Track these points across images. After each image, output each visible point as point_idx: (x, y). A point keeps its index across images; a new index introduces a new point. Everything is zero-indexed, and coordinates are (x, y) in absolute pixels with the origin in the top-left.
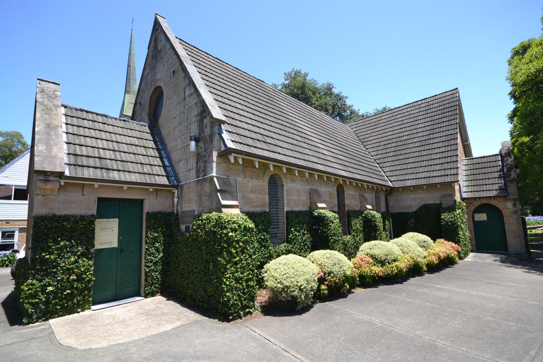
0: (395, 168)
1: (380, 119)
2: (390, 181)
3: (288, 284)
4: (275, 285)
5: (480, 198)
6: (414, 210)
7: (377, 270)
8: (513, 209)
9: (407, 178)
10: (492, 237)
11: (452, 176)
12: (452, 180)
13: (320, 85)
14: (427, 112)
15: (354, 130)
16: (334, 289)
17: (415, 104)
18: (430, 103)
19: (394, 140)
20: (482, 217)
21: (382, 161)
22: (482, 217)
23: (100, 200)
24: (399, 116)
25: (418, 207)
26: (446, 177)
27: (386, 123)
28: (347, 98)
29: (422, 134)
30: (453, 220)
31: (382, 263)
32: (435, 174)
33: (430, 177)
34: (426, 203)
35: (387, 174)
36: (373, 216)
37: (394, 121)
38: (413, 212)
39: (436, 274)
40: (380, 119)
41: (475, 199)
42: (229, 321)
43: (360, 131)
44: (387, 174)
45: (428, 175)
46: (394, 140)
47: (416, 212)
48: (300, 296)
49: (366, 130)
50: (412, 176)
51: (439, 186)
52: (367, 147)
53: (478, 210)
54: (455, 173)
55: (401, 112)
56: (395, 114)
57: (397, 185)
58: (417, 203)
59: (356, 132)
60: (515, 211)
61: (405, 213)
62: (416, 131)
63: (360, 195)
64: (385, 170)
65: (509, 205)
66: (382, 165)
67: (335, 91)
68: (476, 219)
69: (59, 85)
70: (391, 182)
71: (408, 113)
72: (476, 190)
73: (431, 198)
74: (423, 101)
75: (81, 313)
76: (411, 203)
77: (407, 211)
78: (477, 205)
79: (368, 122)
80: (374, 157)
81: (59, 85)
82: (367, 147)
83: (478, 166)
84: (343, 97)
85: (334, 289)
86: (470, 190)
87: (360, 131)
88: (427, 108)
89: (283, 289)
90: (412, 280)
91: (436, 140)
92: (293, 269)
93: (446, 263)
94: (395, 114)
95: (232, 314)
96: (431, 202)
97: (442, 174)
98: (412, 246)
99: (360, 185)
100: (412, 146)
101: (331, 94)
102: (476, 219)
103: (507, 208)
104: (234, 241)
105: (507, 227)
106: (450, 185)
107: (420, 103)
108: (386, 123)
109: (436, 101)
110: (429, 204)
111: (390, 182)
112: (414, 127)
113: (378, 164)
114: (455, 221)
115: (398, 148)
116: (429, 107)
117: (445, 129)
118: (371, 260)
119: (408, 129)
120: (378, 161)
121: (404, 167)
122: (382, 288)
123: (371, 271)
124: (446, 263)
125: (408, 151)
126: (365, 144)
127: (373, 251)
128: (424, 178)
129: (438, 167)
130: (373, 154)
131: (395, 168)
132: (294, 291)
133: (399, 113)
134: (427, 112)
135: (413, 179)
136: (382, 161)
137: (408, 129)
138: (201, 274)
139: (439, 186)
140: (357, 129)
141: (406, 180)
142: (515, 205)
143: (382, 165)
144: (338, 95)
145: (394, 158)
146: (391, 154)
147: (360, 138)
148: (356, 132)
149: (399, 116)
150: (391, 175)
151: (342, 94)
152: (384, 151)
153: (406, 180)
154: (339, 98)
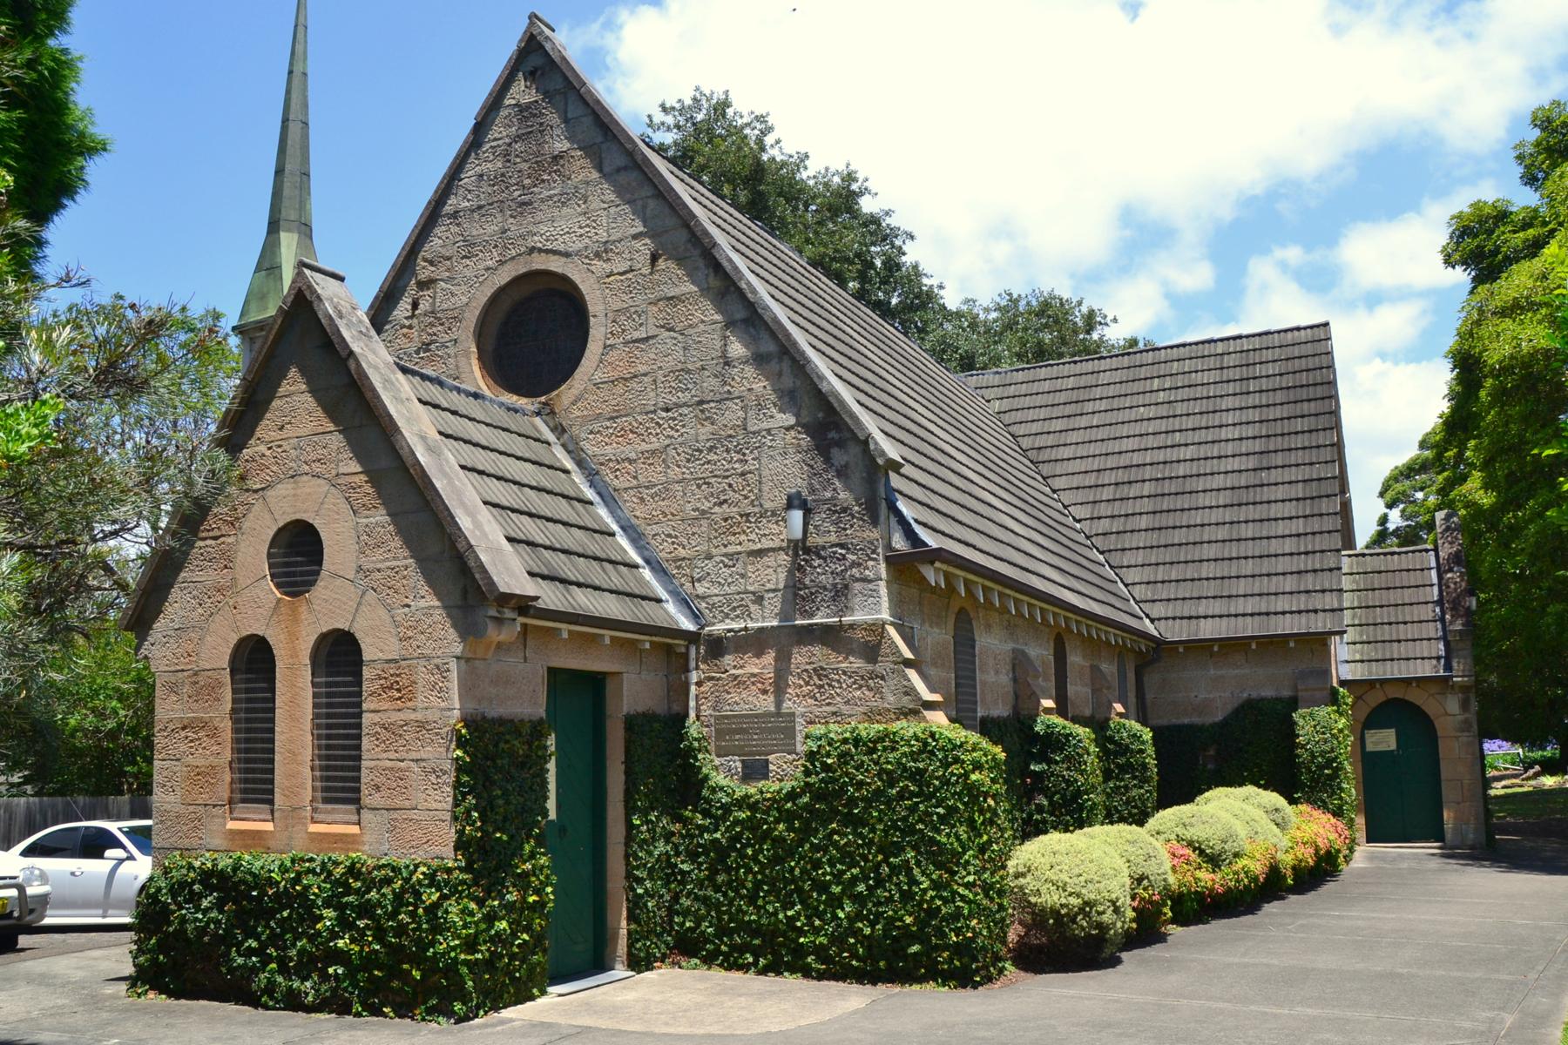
0: (1161, 574)
1: (1090, 380)
2: (1147, 616)
3: (1092, 896)
4: (1063, 901)
5: (1383, 682)
6: (1219, 717)
7: (1206, 878)
8: (1461, 718)
9: (1201, 611)
10: (1402, 802)
11: (1328, 615)
12: (1329, 627)
13: (811, 172)
14: (1244, 387)
15: (997, 405)
16: (1159, 916)
17: (1207, 350)
18: (1252, 357)
19: (1148, 473)
20: (1384, 740)
21: (1112, 542)
22: (1384, 740)
23: (552, 671)
24: (1156, 383)
25: (1229, 708)
26: (1312, 615)
27: (1116, 403)
28: (912, 238)
29: (1235, 464)
30: (1327, 747)
31: (1214, 861)
32: (1282, 604)
33: (1267, 614)
34: (1254, 695)
35: (1137, 591)
36: (1136, 737)
37: (1140, 399)
38: (1213, 725)
39: (1311, 895)
40: (1090, 380)
41: (1371, 684)
42: (975, 986)
43: (1019, 416)
44: (1138, 591)
45: (1263, 605)
46: (1148, 473)
47: (1225, 723)
48: (1114, 924)
49: (1043, 413)
50: (1217, 607)
51: (1292, 644)
52: (1058, 483)
53: (1373, 720)
54: (1336, 606)
55: (1163, 369)
56: (1143, 372)
57: (1175, 632)
58: (1227, 694)
59: (1007, 418)
60: (1466, 721)
61: (1191, 727)
62: (1215, 450)
63: (1092, 667)
64: (1132, 576)
65: (1453, 704)
66: (1116, 559)
67: (867, 205)
68: (1370, 748)
69: (342, 279)
70: (1152, 621)
71: (1186, 380)
72: (1373, 655)
73: (1264, 682)
74: (1232, 346)
75: (539, 1001)
76: (1212, 696)
77: (1196, 720)
78: (1373, 705)
79: (1046, 386)
80: (1085, 526)
81: (342, 279)
82: (1058, 483)
83: (1377, 581)
84: (894, 232)
85: (1159, 916)
86: (1358, 657)
87: (1019, 416)
88: (1245, 372)
89: (1082, 910)
90: (1271, 908)
91: (1280, 492)
92: (1082, 863)
93: (1319, 872)
94: (1143, 372)
95: (977, 971)
96: (1268, 693)
97: (1302, 607)
98: (1244, 820)
99: (1066, 629)
100: (1207, 500)
101: (854, 212)
102: (1370, 748)
103: (1449, 713)
104: (980, 793)
105: (1446, 772)
106: (1318, 643)
107: (1220, 348)
108: (1116, 403)
109: (1269, 355)
110: (1262, 699)
111: (1147, 621)
112: (1137, 387)
113: (1102, 553)
114: (1332, 750)
115: (1166, 504)
116: (1250, 372)
117: (1299, 457)
118: (1194, 856)
119: (1191, 437)
120: (1097, 541)
121: (1190, 571)
122: (1218, 927)
123: (1197, 880)
124: (1319, 872)
125: (1198, 517)
126: (1046, 469)
127: (1192, 830)
128: (1252, 615)
129: (1289, 584)
130: (1079, 512)
131: (1161, 574)
132: (1104, 913)
133: (1154, 371)
134: (1244, 387)
135: (1221, 616)
136: (1112, 542)
137: (1191, 437)
138: (853, 879)
139: (1292, 644)
140: (1006, 404)
141: (1197, 617)
142: (1465, 705)
143: (1116, 559)
144: (874, 220)
145: (1153, 538)
146: (1144, 522)
147: (1026, 443)
148: (1007, 418)
149: (1156, 383)
150: (1150, 596)
151: (892, 221)
152: (1118, 508)
153: (1197, 617)
154: (875, 229)
